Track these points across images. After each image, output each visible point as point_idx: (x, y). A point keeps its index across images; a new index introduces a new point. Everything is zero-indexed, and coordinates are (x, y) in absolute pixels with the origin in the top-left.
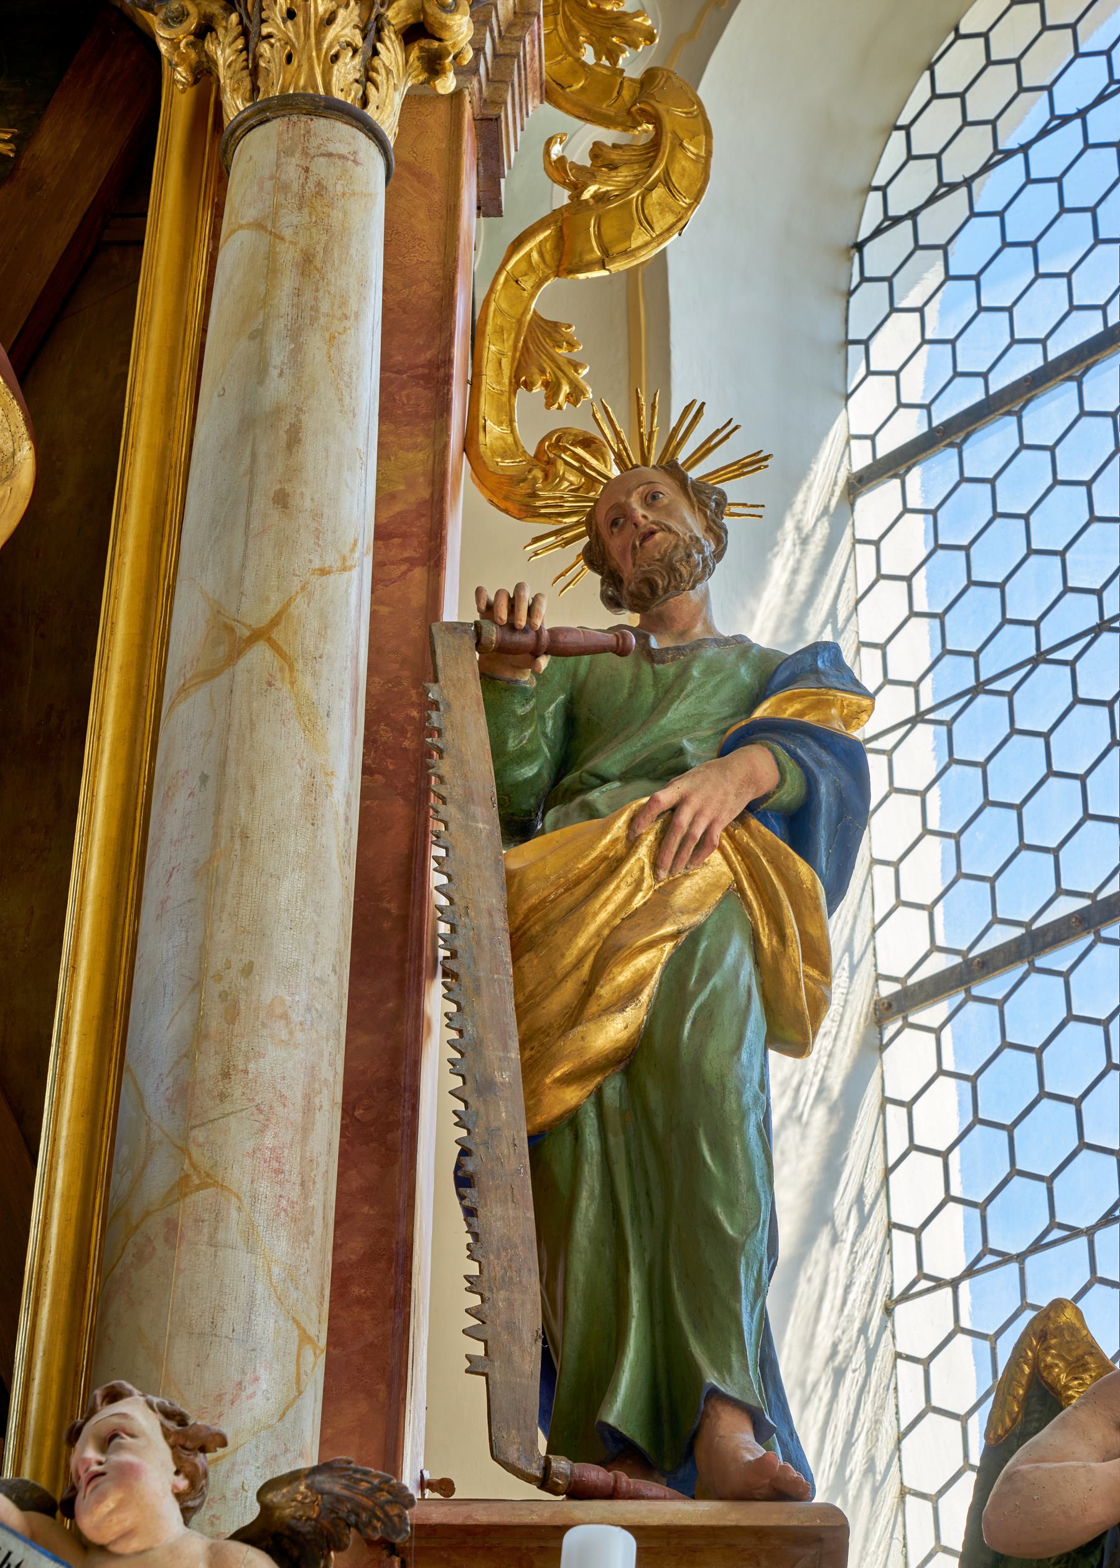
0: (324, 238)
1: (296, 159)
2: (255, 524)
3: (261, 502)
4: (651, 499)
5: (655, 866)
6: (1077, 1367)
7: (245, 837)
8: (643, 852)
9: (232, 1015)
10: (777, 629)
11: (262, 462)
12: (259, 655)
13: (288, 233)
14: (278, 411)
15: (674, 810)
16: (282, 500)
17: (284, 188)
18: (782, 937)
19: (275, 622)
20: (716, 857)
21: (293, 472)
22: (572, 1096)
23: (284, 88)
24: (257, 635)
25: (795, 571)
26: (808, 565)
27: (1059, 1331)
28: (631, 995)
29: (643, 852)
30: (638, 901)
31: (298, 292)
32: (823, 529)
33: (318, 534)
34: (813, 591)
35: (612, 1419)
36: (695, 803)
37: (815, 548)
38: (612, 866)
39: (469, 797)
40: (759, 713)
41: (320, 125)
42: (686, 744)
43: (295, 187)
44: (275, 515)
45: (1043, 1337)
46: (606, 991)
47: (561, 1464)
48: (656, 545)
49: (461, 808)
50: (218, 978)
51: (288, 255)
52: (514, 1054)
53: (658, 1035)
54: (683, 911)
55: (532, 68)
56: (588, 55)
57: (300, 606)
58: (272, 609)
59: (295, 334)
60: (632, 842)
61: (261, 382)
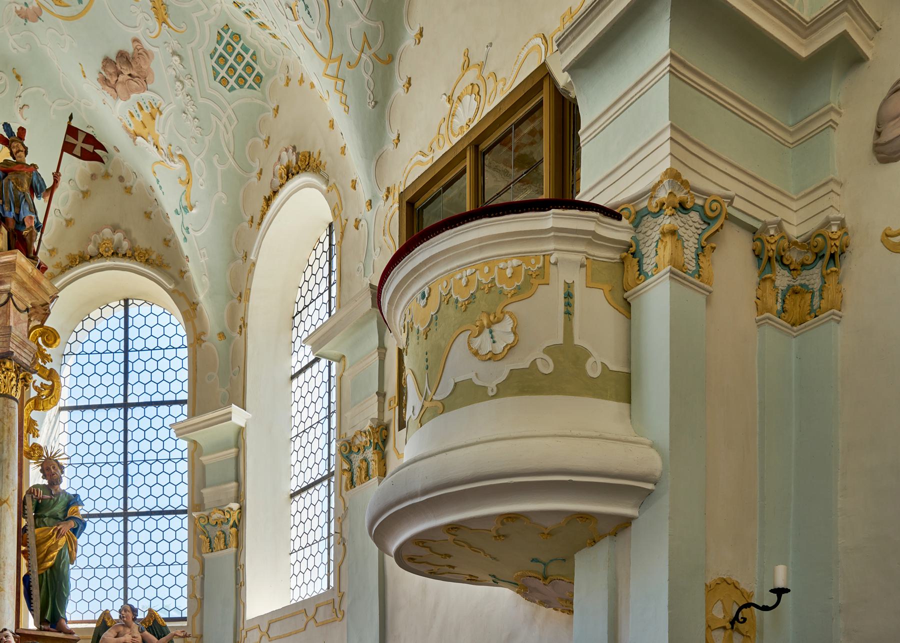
0: (11, 425)
1: (6, 408)
2: (4, 481)
3: (4, 477)
4: (54, 468)
5: (56, 537)
6: (109, 619)
7: (5, 536)
8: (55, 536)
9: (5, 565)
10: (45, 443)
11: (4, 469)
12: (5, 505)
13: (6, 423)
14: (6, 460)
15: (60, 530)
16: (7, 477)
17: (4, 413)
18: (72, 549)
19: (7, 500)
20: (64, 537)
21: (8, 472)
22: (43, 572)
23: (4, 392)
24: (5, 502)
25: (48, 430)
26: (51, 427)
27: (107, 614)
28: (53, 558)
29: (55, 536)
30: (53, 543)
31: (8, 436)
32: (54, 420)
33: (13, 483)
34: (52, 433)
35: (47, 618)
36: (63, 529)
37: (52, 424)
38: (51, 537)
39: (31, 525)
40: (73, 515)
41: (10, 400)
42: (59, 514)
43: (6, 414)
44: (6, 479)
45: (105, 614)
46: (49, 557)
47: (43, 627)
48: (55, 477)
49: (30, 527)
50: (2, 559)
51: (6, 428)
52: (37, 567)
53: (56, 565)
54: (60, 546)
55: (15, 338)
56: (40, 361)
57: (11, 497)
58: (7, 497)
59: (8, 445)
60: (53, 534)
61: (3, 453)
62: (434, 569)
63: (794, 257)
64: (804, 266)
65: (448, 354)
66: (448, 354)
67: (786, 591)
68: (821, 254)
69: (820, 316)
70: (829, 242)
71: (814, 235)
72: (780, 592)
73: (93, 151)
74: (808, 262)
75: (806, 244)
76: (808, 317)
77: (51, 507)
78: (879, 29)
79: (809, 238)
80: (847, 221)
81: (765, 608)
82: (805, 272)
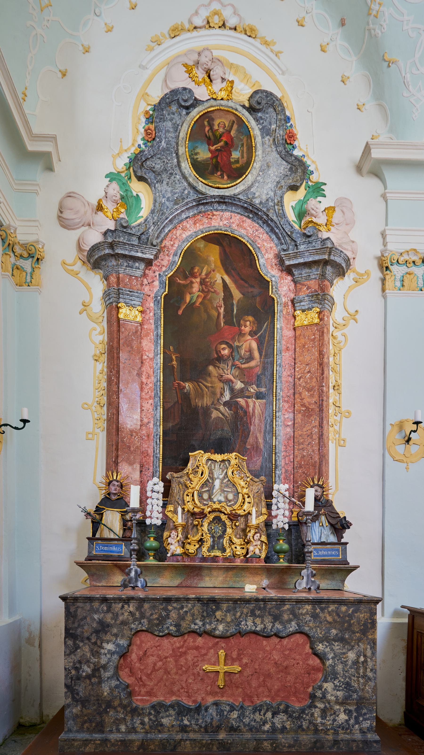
62: (270, 256)
63: (18, 249)
64: (21, 256)
65: (41, 597)
66: (41, 597)
67: (28, 421)
68: (32, 255)
69: (31, 287)
70: (38, 252)
71: (29, 244)
72: (25, 421)
73: (149, 549)
74: (24, 256)
75: (24, 246)
76: (24, 284)
77: (221, 415)
78: (60, 161)
79: (27, 244)
80: (46, 245)
81: (16, 428)
82: (21, 260)
